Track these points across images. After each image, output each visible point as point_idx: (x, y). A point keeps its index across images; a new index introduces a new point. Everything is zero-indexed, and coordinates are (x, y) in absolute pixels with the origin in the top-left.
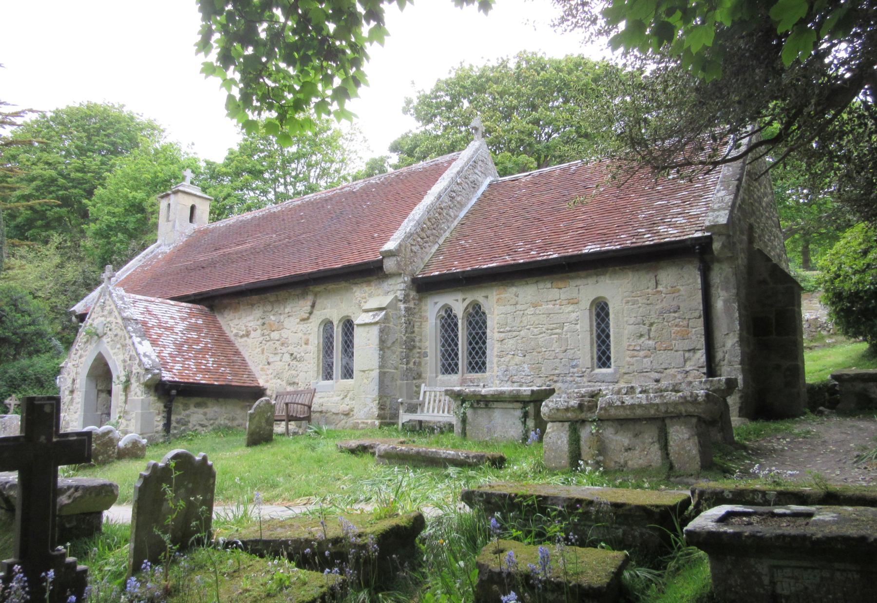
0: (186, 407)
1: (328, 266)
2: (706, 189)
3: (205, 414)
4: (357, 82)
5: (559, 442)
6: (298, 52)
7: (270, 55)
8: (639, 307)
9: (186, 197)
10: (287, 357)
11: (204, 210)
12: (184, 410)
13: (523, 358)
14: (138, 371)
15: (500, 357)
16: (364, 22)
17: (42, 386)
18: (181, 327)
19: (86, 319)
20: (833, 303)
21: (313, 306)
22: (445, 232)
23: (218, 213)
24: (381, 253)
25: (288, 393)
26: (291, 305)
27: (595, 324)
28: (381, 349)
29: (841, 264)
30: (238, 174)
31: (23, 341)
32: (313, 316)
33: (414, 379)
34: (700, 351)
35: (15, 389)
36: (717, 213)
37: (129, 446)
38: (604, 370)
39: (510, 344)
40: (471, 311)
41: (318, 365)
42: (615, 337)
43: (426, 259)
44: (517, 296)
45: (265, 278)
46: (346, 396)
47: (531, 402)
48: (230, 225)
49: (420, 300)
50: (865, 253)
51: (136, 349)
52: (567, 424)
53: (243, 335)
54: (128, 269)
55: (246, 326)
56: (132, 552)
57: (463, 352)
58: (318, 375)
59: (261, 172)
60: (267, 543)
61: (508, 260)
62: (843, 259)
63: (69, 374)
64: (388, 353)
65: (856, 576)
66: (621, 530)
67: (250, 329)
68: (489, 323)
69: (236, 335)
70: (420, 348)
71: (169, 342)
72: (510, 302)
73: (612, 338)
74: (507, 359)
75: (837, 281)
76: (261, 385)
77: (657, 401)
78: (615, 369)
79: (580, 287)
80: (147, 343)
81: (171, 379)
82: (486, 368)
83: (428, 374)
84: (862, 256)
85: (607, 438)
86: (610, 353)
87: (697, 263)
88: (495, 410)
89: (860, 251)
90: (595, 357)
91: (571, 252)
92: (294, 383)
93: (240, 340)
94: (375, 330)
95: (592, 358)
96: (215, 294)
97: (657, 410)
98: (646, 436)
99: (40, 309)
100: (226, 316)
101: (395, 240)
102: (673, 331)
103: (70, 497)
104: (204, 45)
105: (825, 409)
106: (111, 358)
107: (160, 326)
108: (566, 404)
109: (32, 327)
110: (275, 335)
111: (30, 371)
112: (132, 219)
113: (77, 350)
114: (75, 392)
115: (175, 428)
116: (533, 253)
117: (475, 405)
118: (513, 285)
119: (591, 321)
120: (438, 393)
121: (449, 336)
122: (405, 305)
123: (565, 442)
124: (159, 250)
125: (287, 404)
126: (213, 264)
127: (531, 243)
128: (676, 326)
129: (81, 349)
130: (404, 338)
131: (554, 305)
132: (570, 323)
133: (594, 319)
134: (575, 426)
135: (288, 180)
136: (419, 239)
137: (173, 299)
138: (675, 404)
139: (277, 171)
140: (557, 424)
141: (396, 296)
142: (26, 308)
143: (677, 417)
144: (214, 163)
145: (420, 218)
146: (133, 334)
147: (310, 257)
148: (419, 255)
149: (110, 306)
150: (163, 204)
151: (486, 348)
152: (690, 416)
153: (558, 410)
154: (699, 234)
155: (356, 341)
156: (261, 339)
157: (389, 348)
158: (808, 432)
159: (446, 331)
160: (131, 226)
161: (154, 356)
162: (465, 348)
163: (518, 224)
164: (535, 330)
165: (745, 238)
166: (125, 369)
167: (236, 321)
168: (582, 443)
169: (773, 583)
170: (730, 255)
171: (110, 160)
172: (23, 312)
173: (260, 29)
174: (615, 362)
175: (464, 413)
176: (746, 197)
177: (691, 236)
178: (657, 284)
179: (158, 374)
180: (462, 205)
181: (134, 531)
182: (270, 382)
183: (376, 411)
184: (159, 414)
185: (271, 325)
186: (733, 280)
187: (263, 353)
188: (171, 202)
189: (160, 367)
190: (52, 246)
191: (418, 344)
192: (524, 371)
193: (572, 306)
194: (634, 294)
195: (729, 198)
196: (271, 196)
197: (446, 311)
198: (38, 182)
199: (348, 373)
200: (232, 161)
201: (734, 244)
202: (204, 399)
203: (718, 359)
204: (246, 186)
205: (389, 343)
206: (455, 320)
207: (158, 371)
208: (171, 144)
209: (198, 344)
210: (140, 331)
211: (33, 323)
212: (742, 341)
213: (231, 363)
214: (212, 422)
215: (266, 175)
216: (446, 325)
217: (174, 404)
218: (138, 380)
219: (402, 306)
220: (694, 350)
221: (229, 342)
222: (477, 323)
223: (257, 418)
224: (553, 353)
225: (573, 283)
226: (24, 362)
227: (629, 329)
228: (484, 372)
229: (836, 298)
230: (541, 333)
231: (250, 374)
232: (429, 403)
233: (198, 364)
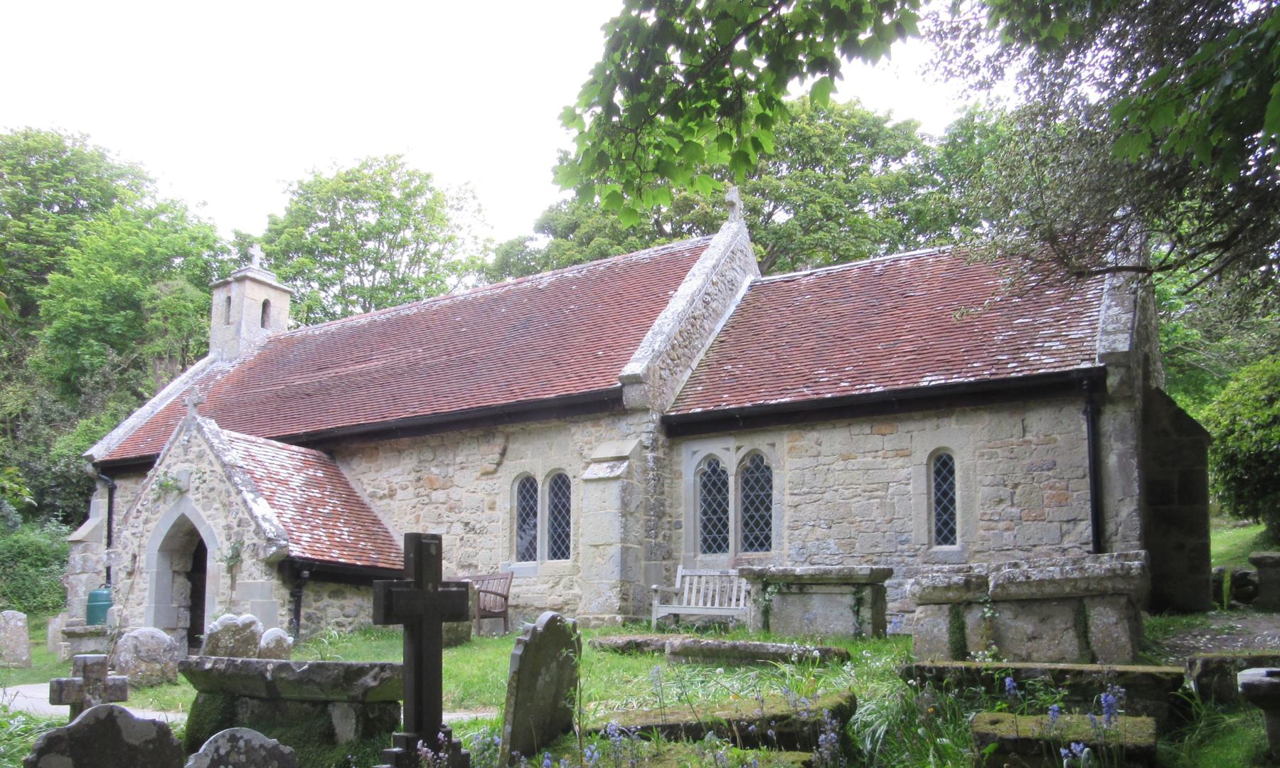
1: (532, 396)
2: (1087, 305)
3: (342, 608)
5: (936, 630)
8: (999, 462)
14: (254, 541)
18: (297, 480)
19: (156, 465)
21: (503, 454)
22: (698, 352)
24: (620, 379)
26: (466, 452)
27: (933, 484)
28: (623, 516)
29: (1234, 415)
32: (502, 468)
33: (664, 559)
34: (1083, 523)
36: (1112, 337)
37: (272, 645)
38: (946, 548)
39: (808, 511)
40: (748, 465)
43: (678, 390)
44: (820, 445)
45: (428, 411)
46: (557, 583)
47: (866, 584)
49: (671, 447)
50: (1271, 401)
51: (250, 511)
52: (946, 608)
53: (384, 495)
54: (169, 395)
55: (388, 483)
58: (511, 553)
61: (808, 393)
62: (1240, 408)
63: (126, 547)
67: (395, 486)
69: (373, 495)
70: (671, 516)
71: (284, 498)
72: (809, 453)
75: (1230, 439)
77: (1076, 575)
78: (962, 546)
79: (915, 434)
80: (261, 501)
81: (301, 555)
82: (770, 545)
83: (683, 553)
84: (1266, 405)
85: (1004, 624)
86: (955, 524)
88: (814, 596)
89: (1263, 397)
90: (934, 529)
91: (901, 384)
92: (470, 566)
93: (379, 503)
94: (615, 488)
95: (930, 532)
96: (341, 433)
98: (1057, 621)
100: (354, 467)
101: (638, 360)
102: (1045, 495)
103: (375, 678)
105: (1238, 604)
106: (203, 522)
107: (271, 480)
108: (947, 580)
110: (439, 496)
113: (138, 511)
115: (306, 627)
116: (843, 384)
117: (785, 590)
118: (813, 429)
120: (696, 579)
122: (653, 454)
123: (944, 630)
124: (215, 367)
126: (324, 389)
128: (1051, 488)
129: (147, 510)
130: (652, 501)
131: (874, 457)
133: (932, 479)
134: (957, 610)
136: (669, 361)
138: (1100, 579)
140: (932, 606)
141: (641, 441)
144: (249, 236)
145: (670, 332)
146: (243, 488)
148: (669, 383)
149: (199, 446)
151: (770, 516)
152: (1117, 593)
153: (935, 588)
156: (416, 500)
157: (631, 514)
158: (1232, 628)
159: (709, 492)
162: (739, 517)
164: (846, 492)
166: (229, 539)
167: (372, 475)
168: (968, 631)
174: (962, 536)
177: (1076, 367)
178: (1024, 430)
180: (718, 315)
181: (512, 710)
183: (617, 603)
184: (283, 606)
185: (431, 481)
186: (1131, 427)
188: (233, 295)
192: (828, 549)
193: (902, 459)
194: (991, 444)
197: (710, 465)
199: (560, 548)
203: (1108, 534)
206: (724, 477)
207: (285, 542)
209: (324, 506)
210: (250, 484)
213: (371, 536)
214: (350, 620)
216: (709, 485)
217: (305, 592)
218: (255, 553)
220: (1075, 521)
221: (362, 505)
224: (873, 525)
227: (983, 492)
228: (767, 550)
229: (1226, 461)
230: (856, 496)
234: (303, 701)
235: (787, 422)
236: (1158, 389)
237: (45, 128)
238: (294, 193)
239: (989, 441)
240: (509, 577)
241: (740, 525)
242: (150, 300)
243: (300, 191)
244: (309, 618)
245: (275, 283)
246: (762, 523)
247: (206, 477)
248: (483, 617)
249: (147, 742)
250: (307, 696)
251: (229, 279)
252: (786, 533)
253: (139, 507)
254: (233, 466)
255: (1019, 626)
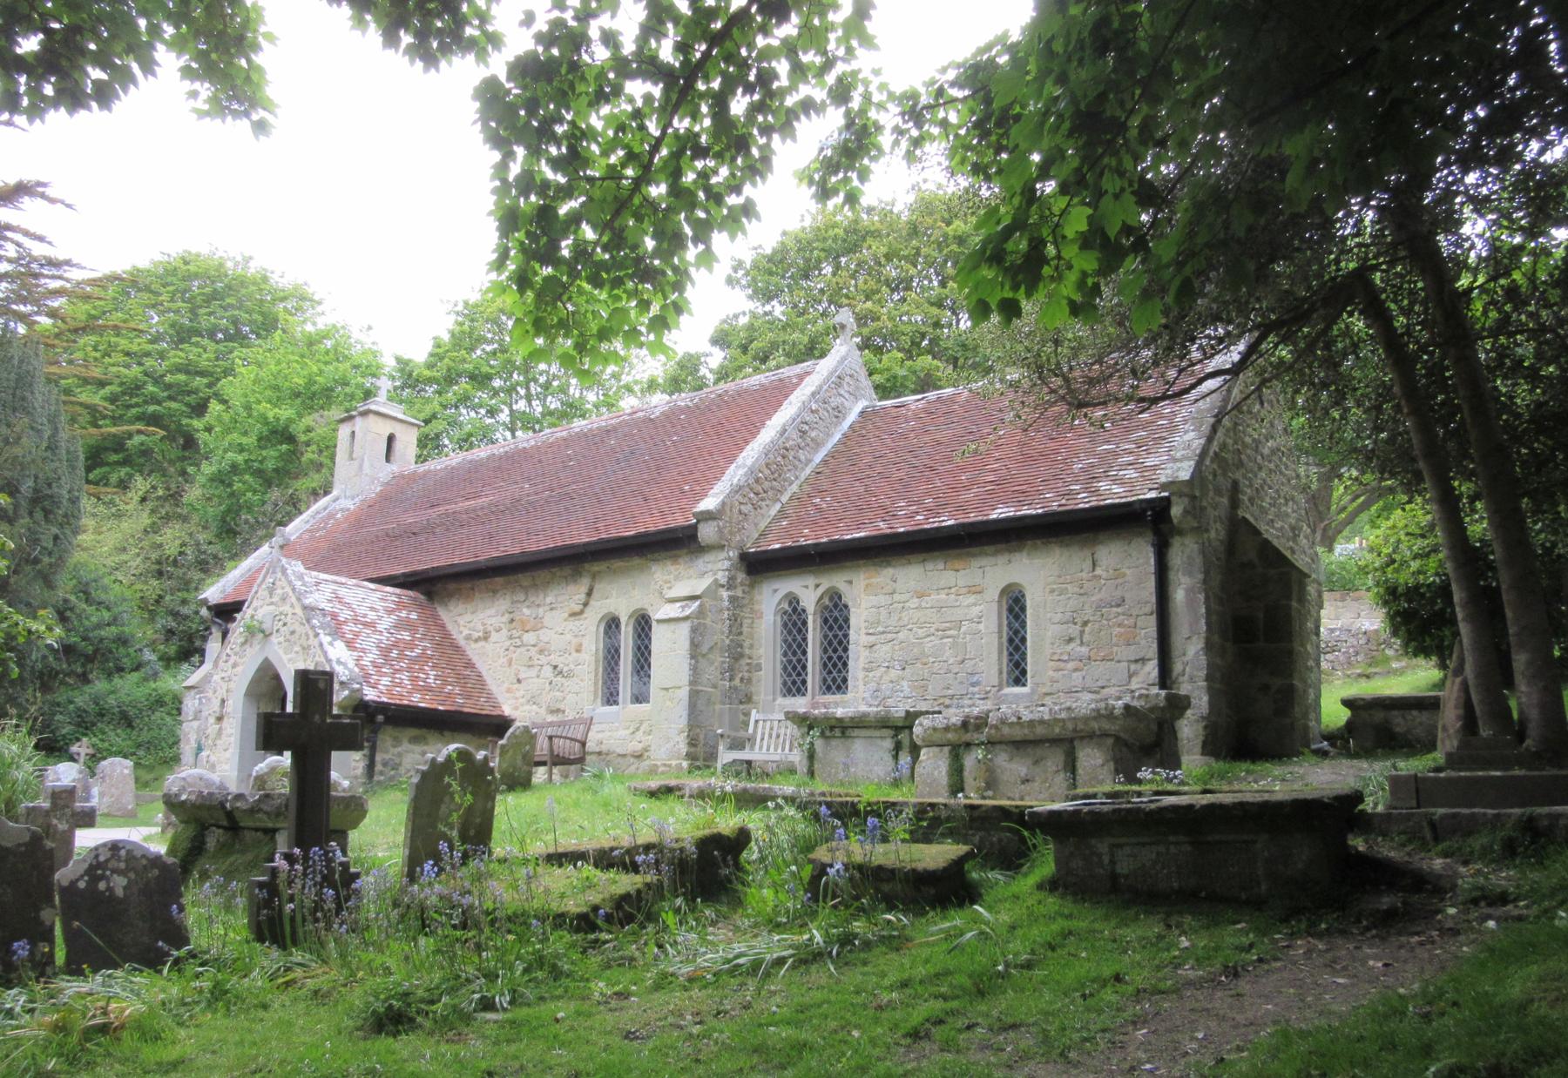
0: (397, 741)
1: (614, 533)
2: (1172, 428)
4: (678, 309)
5: (936, 773)
6: (608, 272)
7: (575, 276)
9: (380, 420)
10: (548, 671)
11: (408, 442)
12: (395, 746)
13: (900, 672)
15: (867, 670)
16: (690, 245)
17: (130, 725)
18: (386, 623)
20: (1386, 603)
21: (589, 594)
22: (790, 485)
23: (429, 445)
24: (695, 515)
25: (551, 724)
26: (555, 592)
27: (1005, 622)
28: (692, 657)
30: (450, 380)
31: (96, 651)
32: (588, 610)
33: (741, 703)
35: (87, 728)
36: (1178, 464)
39: (883, 651)
41: (596, 684)
42: (1033, 642)
43: (762, 526)
45: (517, 550)
46: (638, 729)
48: (453, 468)
49: (752, 586)
51: (325, 653)
52: (946, 749)
56: (406, 860)
57: (814, 664)
58: (596, 698)
59: (489, 377)
60: (565, 855)
61: (883, 528)
64: (703, 663)
65: (1189, 848)
66: (978, 837)
68: (853, 621)
69: (468, 638)
70: (750, 658)
71: (369, 642)
73: (1029, 643)
74: (878, 673)
75: (1390, 569)
76: (506, 714)
78: (1032, 689)
79: (986, 569)
80: (340, 644)
87: (1150, 537)
88: (856, 740)
91: (973, 517)
92: (558, 711)
93: (473, 645)
94: (685, 628)
95: (1001, 673)
96: (436, 573)
97: (1063, 728)
98: (1049, 764)
99: (125, 600)
104: (499, 264)
107: (356, 622)
109: (113, 628)
110: (529, 638)
111: (112, 701)
112: (272, 453)
113: (228, 655)
114: (225, 719)
115: (381, 773)
117: (828, 733)
118: (889, 564)
119: (1000, 617)
120: (776, 723)
121: (794, 640)
123: (944, 773)
124: (337, 506)
125: (550, 738)
126: (429, 528)
127: (918, 503)
128: (1119, 625)
129: (236, 654)
130: (727, 642)
132: (971, 621)
134: (957, 751)
135: (533, 391)
136: (752, 495)
137: (372, 580)
138: (1086, 719)
139: (515, 376)
141: (716, 580)
142: (103, 597)
143: (1090, 737)
144: (410, 361)
145: (753, 464)
146: (320, 631)
147: (585, 519)
148: (751, 518)
150: (344, 431)
152: (1105, 735)
153: (935, 729)
154: (1152, 495)
155: (654, 647)
157: (704, 656)
159: (790, 632)
160: (270, 465)
161: (351, 664)
162: (818, 659)
163: (901, 474)
164: (920, 631)
165: (1225, 501)
167: (468, 617)
168: (966, 774)
169: (1113, 862)
170: (1196, 525)
171: (231, 352)
172: (99, 603)
173: (563, 244)
175: (812, 744)
176: (1230, 441)
177: (1141, 497)
178: (1094, 565)
179: (358, 690)
180: (818, 444)
182: (521, 709)
183: (683, 748)
185: (522, 622)
186: (1199, 560)
187: (510, 665)
189: (361, 680)
190: (134, 496)
191: (747, 651)
194: (1061, 580)
195: (1198, 443)
196: (504, 416)
197: (790, 603)
198: (115, 388)
200: (441, 359)
201: (1203, 509)
202: (423, 732)
203: (1175, 674)
204: (465, 399)
205: (704, 649)
206: (804, 616)
208: (334, 326)
209: (412, 650)
210: (329, 626)
211: (114, 621)
212: (1209, 646)
213: (461, 679)
215: (497, 383)
217: (380, 736)
219: (725, 594)
220: (1142, 660)
221: (457, 648)
222: (836, 620)
223: (511, 752)
225: (975, 563)
226: (100, 685)
227: (1053, 631)
228: (844, 693)
231: (490, 697)
232: (762, 739)
233: (414, 679)
234: (257, 830)
235: (863, 557)
236: (1245, 519)
237: (204, 250)
238: (458, 314)
239: (1060, 577)
240: (589, 723)
241: (818, 668)
242: (304, 432)
243: (466, 312)
244: (385, 764)
245: (401, 416)
246: (840, 665)
247: (288, 619)
248: (555, 764)
249: (19, 845)
250: (258, 824)
251: (354, 413)
252: (861, 675)
253: (228, 651)
254: (313, 609)
255: (1012, 767)
